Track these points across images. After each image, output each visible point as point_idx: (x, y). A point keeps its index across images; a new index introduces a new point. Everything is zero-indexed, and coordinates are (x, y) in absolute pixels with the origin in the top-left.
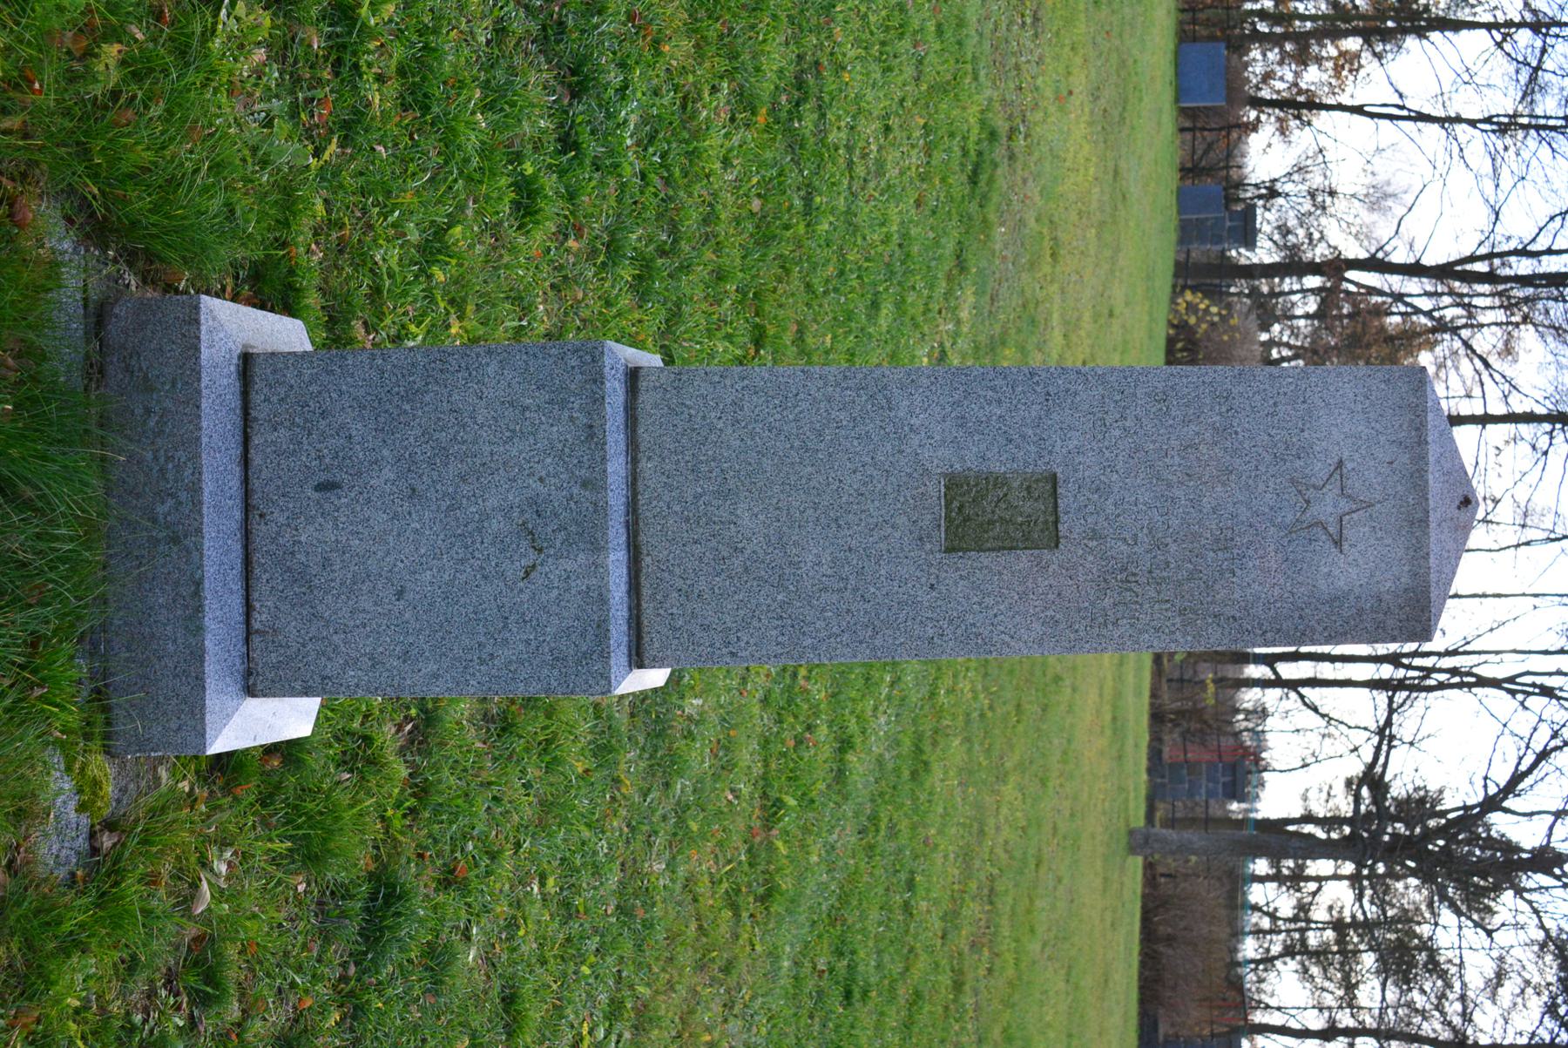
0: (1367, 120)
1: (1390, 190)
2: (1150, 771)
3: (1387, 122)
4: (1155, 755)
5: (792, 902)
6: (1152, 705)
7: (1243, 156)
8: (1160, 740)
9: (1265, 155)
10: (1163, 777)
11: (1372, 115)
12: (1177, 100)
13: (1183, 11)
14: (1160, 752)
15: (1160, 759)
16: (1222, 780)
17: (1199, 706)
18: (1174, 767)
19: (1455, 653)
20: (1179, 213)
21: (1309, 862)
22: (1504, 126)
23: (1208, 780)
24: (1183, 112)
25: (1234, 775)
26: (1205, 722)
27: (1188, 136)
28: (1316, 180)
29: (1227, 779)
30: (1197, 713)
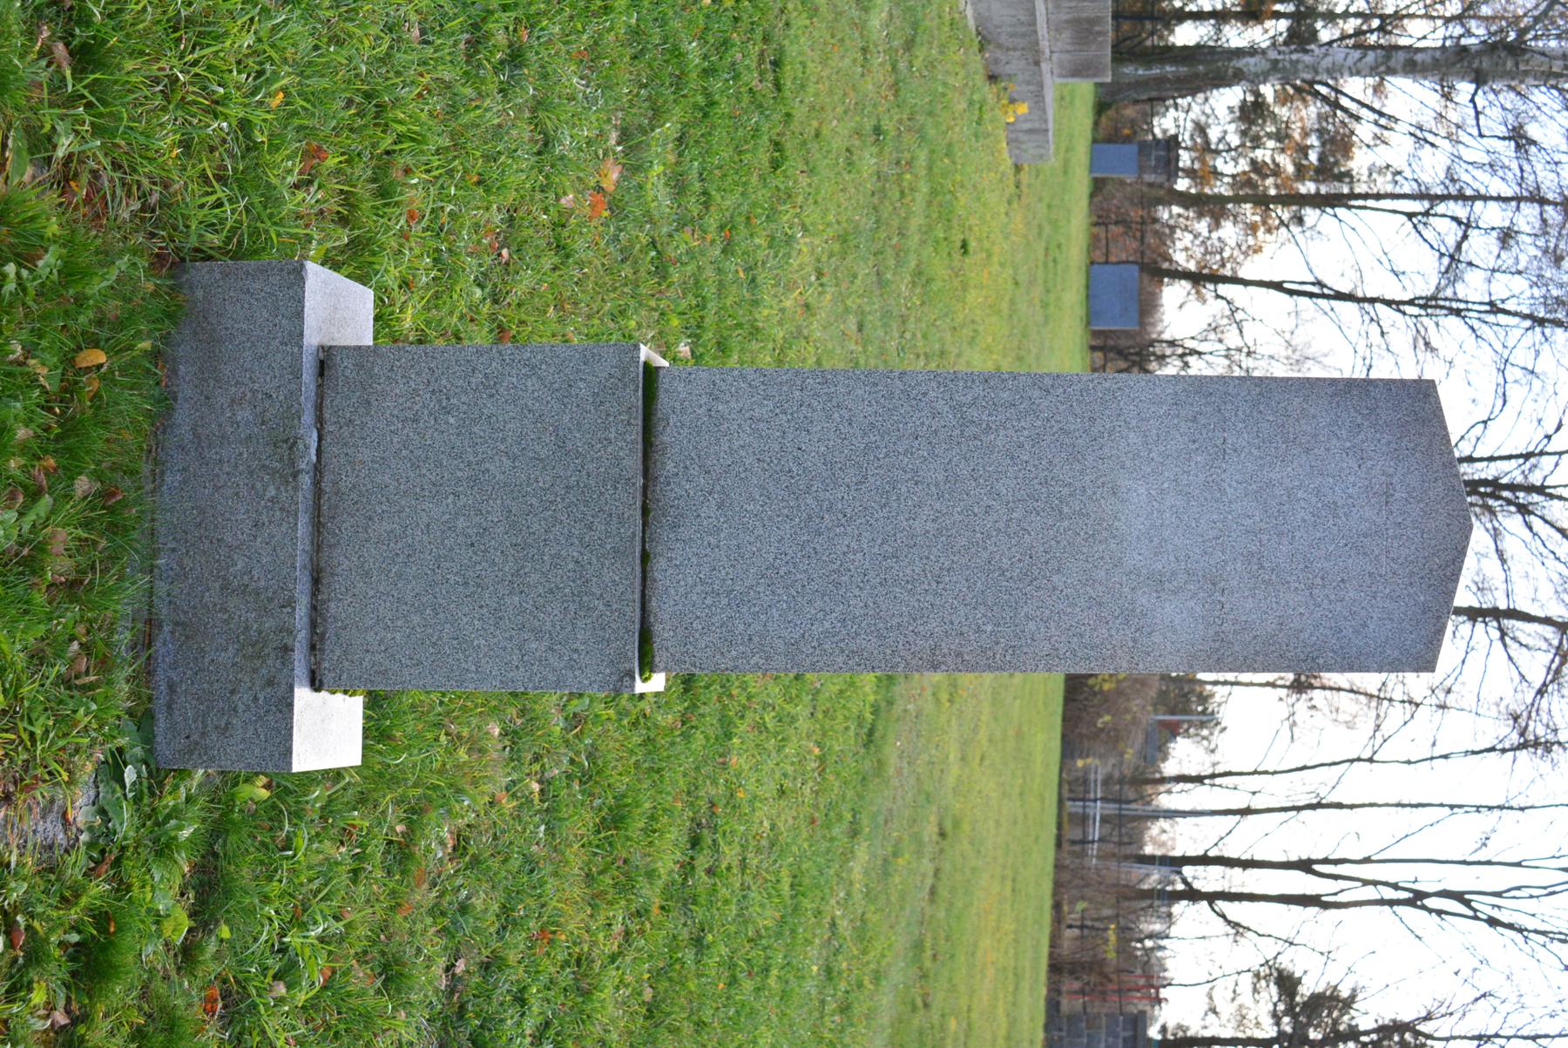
0: (1287, 297)
1: (1309, 352)
2: (1047, 1028)
3: (1306, 300)
4: (1053, 1006)
5: (804, 143)
6: (1051, 955)
7: (1154, 325)
8: (1059, 992)
9: (1180, 313)
10: (1060, 1030)
11: (1291, 293)
12: (1088, 323)
13: (1093, 348)
14: (1058, 1003)
15: (1058, 1010)
16: (1123, 1034)
17: (1101, 956)
18: (1072, 1019)
19: (1367, 860)
20: (1091, 171)
21: (1181, 164)
22: (1429, 303)
23: (1108, 1034)
24: (1096, 334)
25: (1135, 1030)
26: (1106, 977)
27: (1099, 354)
28: (1233, 339)
29: (1128, 1034)
30: (1096, 966)
